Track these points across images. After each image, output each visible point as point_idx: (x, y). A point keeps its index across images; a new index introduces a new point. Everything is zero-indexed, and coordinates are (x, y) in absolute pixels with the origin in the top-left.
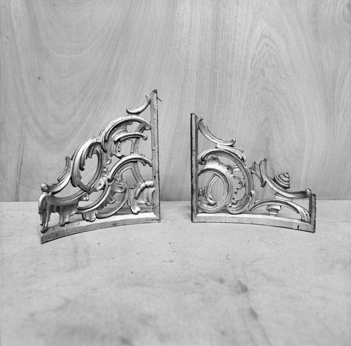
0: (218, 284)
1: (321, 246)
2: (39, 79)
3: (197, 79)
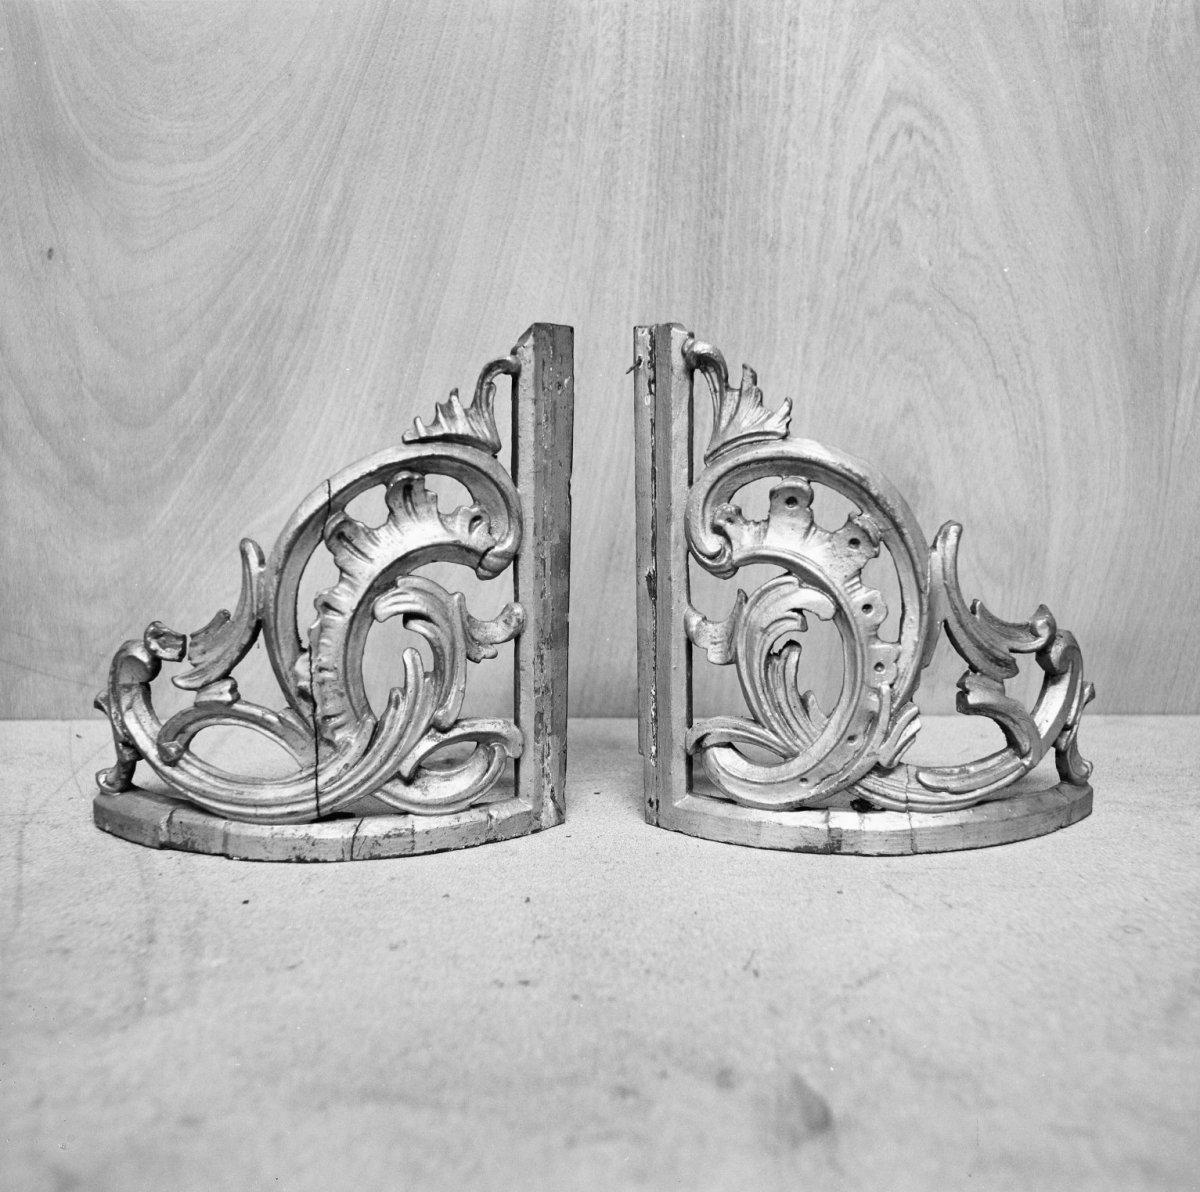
0: (708, 1093)
1: (1125, 912)
2: (50, 257)
3: (647, 257)
